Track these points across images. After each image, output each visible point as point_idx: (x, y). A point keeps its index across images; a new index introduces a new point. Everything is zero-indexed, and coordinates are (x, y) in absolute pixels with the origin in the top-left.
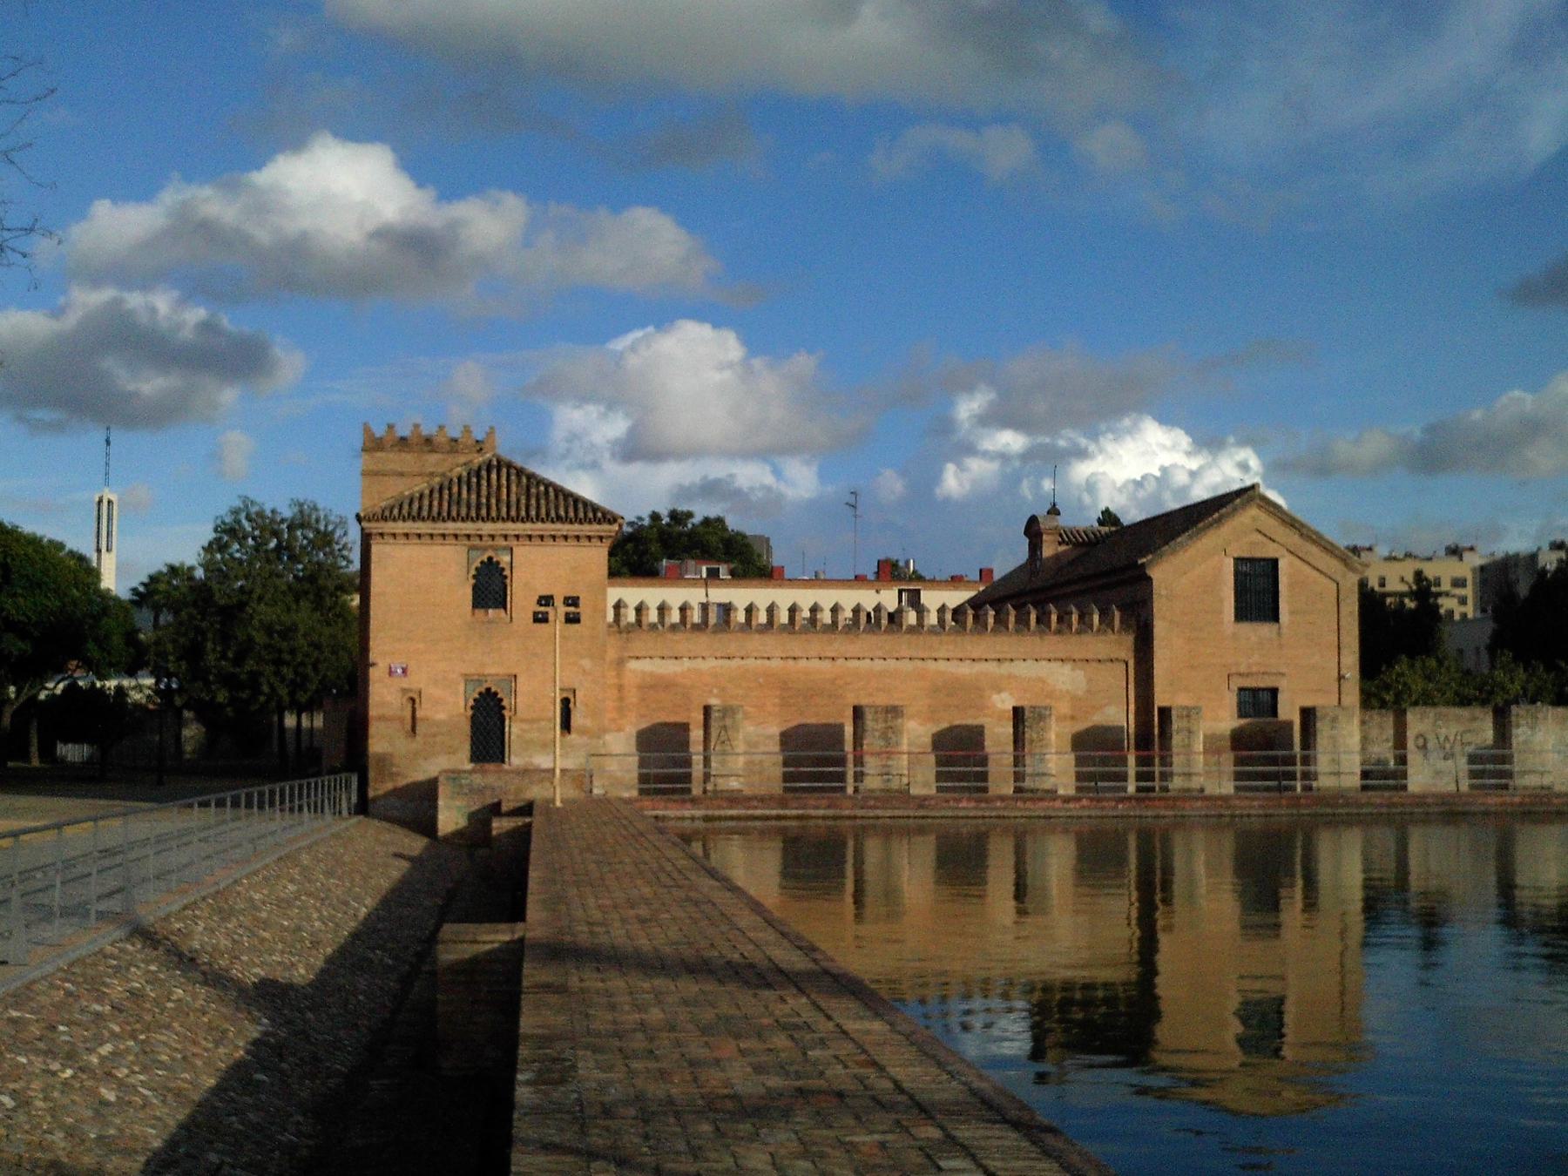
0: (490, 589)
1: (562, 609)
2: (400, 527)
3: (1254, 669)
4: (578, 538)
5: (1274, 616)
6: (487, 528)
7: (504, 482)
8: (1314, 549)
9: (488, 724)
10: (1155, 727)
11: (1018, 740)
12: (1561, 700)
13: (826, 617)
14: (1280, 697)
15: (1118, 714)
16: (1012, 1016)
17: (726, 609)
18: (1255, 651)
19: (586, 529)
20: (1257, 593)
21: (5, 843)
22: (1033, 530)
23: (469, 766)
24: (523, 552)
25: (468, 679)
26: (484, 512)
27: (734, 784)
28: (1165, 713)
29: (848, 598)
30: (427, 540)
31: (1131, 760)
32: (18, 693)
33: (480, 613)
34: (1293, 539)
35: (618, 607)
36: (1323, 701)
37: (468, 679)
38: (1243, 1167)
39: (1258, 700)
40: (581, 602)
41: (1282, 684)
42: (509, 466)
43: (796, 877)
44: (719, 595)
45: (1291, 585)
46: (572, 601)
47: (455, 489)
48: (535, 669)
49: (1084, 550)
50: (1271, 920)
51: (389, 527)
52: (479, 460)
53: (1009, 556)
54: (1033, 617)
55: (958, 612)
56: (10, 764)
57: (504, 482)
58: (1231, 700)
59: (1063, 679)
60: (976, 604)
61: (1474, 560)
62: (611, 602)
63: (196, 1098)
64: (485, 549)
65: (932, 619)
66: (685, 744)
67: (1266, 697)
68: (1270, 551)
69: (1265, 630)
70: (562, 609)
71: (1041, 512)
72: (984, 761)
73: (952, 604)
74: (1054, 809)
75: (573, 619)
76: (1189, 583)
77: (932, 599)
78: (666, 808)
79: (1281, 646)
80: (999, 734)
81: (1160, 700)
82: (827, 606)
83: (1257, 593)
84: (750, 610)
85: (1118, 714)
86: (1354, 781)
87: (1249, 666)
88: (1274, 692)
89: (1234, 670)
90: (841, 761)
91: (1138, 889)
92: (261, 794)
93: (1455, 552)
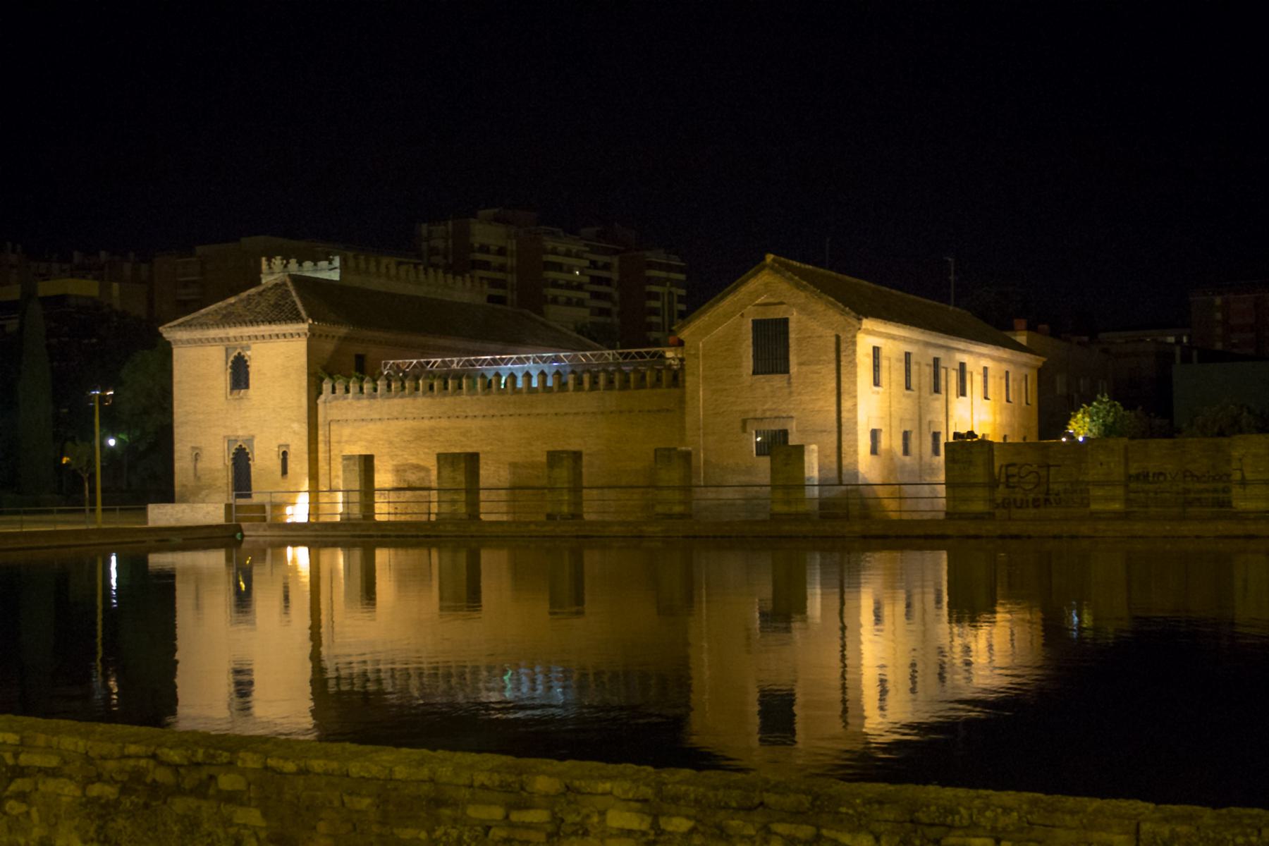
3: (768, 414)
4: (284, 335)
12: (1261, 430)
16: (973, 646)
21: (1141, 845)
25: (230, 441)
27: (800, 762)
30: (275, 339)
32: (103, 446)
37: (230, 441)
38: (877, 383)
43: (449, 608)
45: (799, 341)
50: (240, 677)
56: (114, 559)
63: (460, 698)
68: (777, 313)
74: (327, 756)
78: (22, 523)
79: (790, 393)
86: (942, 516)
87: (764, 411)
89: (751, 415)
91: (434, 750)
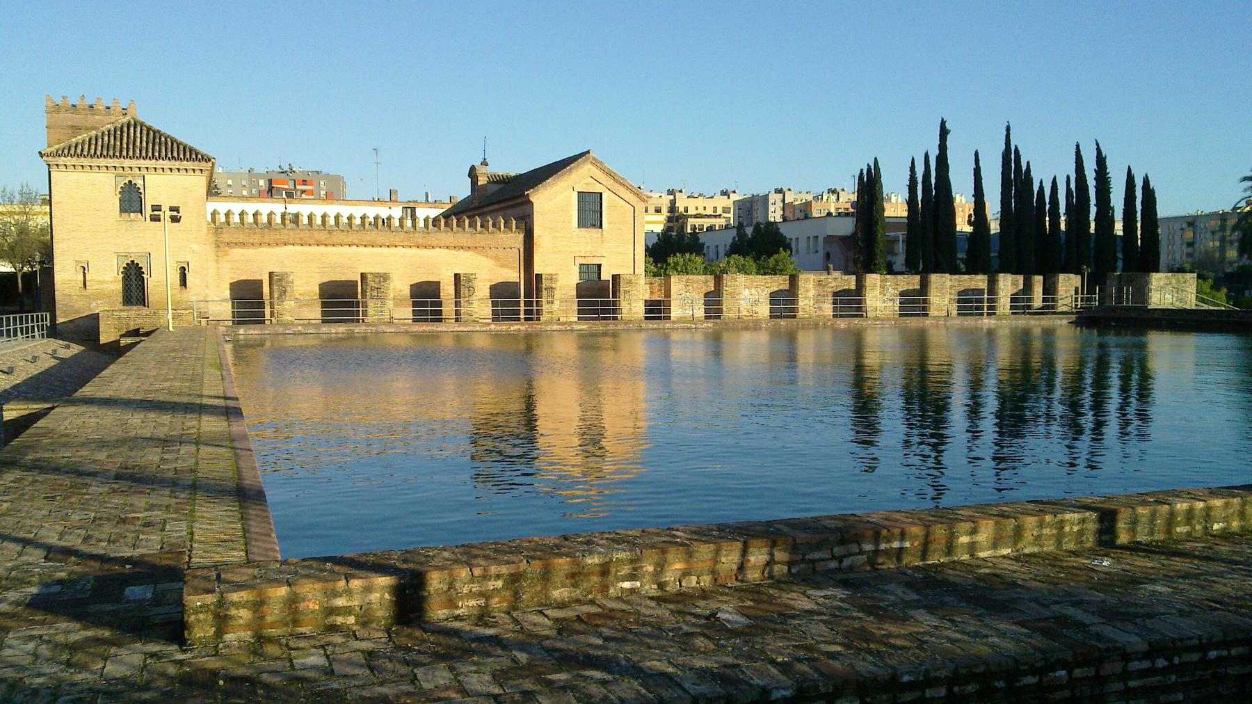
0: (131, 199)
1: (168, 213)
2: (70, 161)
5: (601, 227)
6: (127, 163)
7: (138, 134)
8: (621, 188)
9: (134, 283)
10: (534, 284)
11: (458, 293)
13: (236, 219)
14: (602, 269)
15: (513, 275)
17: (297, 216)
18: (588, 245)
19: (189, 165)
20: (591, 211)
22: (472, 173)
23: (121, 307)
24: (151, 179)
25: (118, 255)
26: (124, 153)
28: (539, 276)
29: (372, 212)
31: (522, 304)
33: (125, 215)
34: (609, 182)
35: (214, 214)
36: (625, 271)
37: (118, 255)
39: (591, 271)
40: (181, 210)
41: (603, 262)
42: (142, 125)
44: (293, 208)
45: (609, 207)
46: (176, 209)
47: (106, 138)
48: (162, 250)
49: (500, 186)
51: (62, 161)
52: (125, 120)
53: (463, 191)
54: (467, 221)
55: (436, 221)
57: (138, 134)
58: (576, 270)
59: (484, 261)
60: (446, 215)
61: (734, 197)
62: (210, 210)
64: (126, 176)
65: (421, 224)
66: (261, 295)
67: (596, 269)
68: (597, 188)
69: (594, 232)
70: (168, 213)
71: (477, 164)
72: (440, 304)
73: (432, 216)
75: (175, 220)
76: (553, 205)
77: (422, 213)
80: (447, 290)
81: (537, 270)
82: (332, 214)
83: (591, 211)
84: (310, 217)
85: (513, 275)
88: (599, 266)
90: (262, 305)
92: (15, 319)
93: (725, 193)
